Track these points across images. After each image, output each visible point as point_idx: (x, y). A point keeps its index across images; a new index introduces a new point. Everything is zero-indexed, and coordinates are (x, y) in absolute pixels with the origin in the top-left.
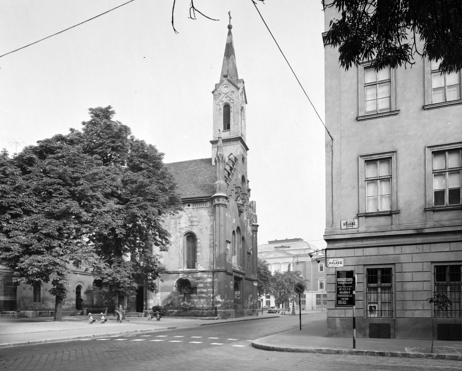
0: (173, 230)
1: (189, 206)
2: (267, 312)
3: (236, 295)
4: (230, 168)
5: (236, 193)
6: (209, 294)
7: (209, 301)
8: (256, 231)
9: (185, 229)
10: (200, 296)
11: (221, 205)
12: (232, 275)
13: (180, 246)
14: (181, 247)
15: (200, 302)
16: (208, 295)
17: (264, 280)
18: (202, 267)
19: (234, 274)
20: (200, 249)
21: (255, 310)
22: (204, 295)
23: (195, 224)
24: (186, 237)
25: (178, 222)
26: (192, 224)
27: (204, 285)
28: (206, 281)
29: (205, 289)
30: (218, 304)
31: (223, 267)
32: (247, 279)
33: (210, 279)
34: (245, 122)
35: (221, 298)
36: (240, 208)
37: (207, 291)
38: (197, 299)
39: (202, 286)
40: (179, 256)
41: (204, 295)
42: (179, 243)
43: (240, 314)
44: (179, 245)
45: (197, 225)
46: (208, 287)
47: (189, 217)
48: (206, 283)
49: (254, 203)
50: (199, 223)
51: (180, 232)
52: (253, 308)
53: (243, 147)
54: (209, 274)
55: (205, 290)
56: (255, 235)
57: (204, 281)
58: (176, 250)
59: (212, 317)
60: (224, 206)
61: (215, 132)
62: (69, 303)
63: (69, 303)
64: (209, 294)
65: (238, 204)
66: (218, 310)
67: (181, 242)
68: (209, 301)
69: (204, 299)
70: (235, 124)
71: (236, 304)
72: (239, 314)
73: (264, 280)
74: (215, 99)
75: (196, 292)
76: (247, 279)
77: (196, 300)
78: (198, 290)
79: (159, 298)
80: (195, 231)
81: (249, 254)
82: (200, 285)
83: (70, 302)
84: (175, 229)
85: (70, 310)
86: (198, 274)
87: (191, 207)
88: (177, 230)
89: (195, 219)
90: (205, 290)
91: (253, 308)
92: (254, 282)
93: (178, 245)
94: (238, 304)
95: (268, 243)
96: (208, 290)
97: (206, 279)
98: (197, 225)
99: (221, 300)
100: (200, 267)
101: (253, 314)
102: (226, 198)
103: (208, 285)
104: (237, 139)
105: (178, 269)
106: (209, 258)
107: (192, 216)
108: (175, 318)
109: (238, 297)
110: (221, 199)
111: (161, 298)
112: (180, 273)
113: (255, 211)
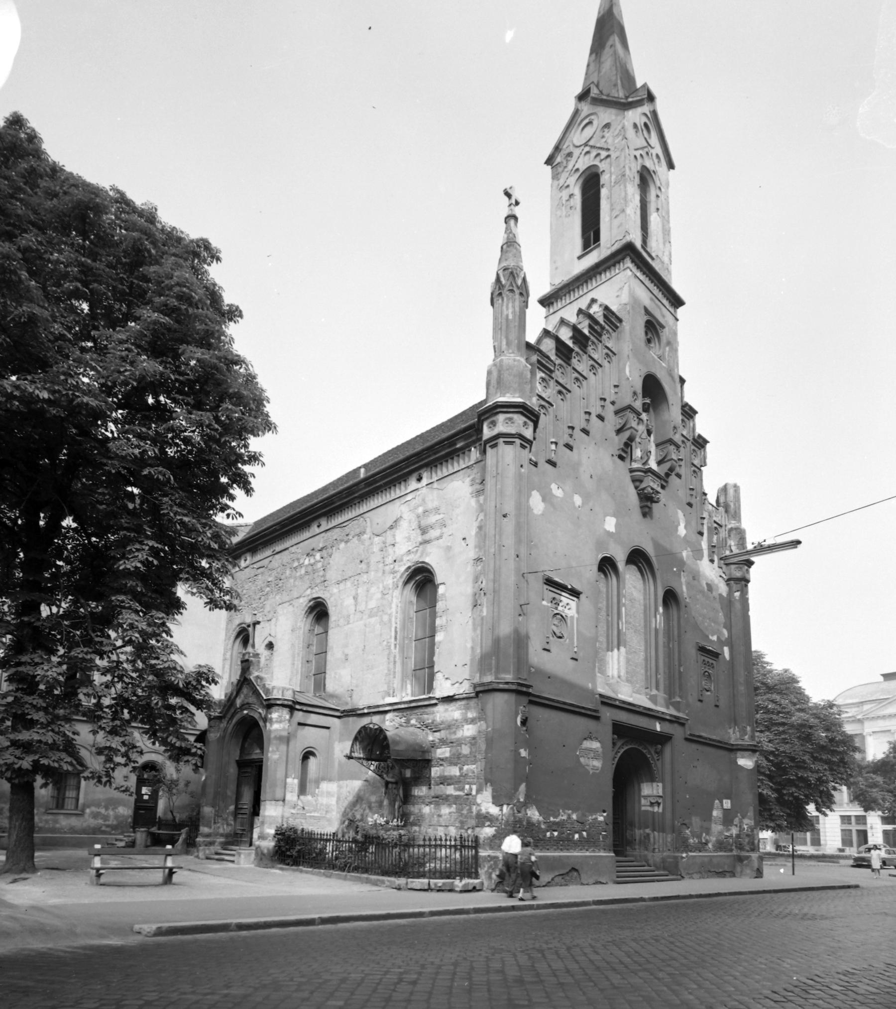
0: (377, 571)
1: (419, 479)
2: (851, 862)
3: (646, 797)
4: (570, 334)
5: (619, 431)
6: (467, 787)
7: (465, 812)
8: (745, 581)
9: (405, 558)
10: (439, 793)
11: (501, 440)
12: (597, 718)
13: (390, 620)
14: (396, 621)
15: (440, 816)
16: (462, 789)
17: (827, 762)
18: (449, 683)
19: (608, 715)
20: (444, 618)
21: (748, 858)
22: (450, 790)
23: (433, 534)
24: (410, 585)
25: (390, 540)
26: (427, 537)
27: (454, 750)
28: (460, 734)
29: (456, 765)
30: (483, 826)
31: (508, 672)
32: (692, 740)
33: (470, 726)
34: (666, 220)
35: (497, 801)
36: (643, 486)
37: (461, 776)
38: (431, 803)
39: (448, 755)
40: (386, 652)
41: (450, 790)
42: (391, 608)
43: (664, 869)
44: (390, 615)
45: (440, 537)
46: (465, 756)
47: (418, 517)
48: (459, 743)
49: (731, 492)
50: (444, 530)
51: (394, 572)
52: (741, 847)
53: (656, 291)
54: (467, 708)
55: (454, 771)
56: (737, 594)
57: (453, 737)
58: (381, 635)
59: (440, 882)
60: (518, 441)
61: (556, 268)
62: (103, 811)
63: (103, 811)
64: (467, 787)
65: (631, 471)
66: (483, 853)
67: (394, 606)
68: (465, 812)
69: (450, 806)
70: (615, 213)
71: (648, 831)
72: (658, 869)
73: (827, 762)
74: (555, 177)
75: (429, 778)
76: (692, 740)
77: (426, 810)
78: (435, 772)
79: (333, 801)
80: (433, 558)
81: (709, 654)
82: (443, 752)
83: (107, 808)
84: (381, 565)
85: (104, 832)
86: (436, 709)
87: (425, 481)
88: (387, 568)
89: (433, 519)
90: (454, 771)
91: (741, 847)
92: (739, 754)
93: (386, 618)
94: (654, 830)
95: (882, 679)
96: (465, 768)
97: (458, 727)
98: (440, 537)
99: (494, 810)
100: (443, 688)
101: (738, 869)
102: (532, 416)
103: (465, 750)
104: (619, 257)
105: (383, 698)
106: (469, 645)
107: (425, 512)
108: (339, 877)
109: (652, 804)
110: (501, 417)
111: (338, 799)
112: (386, 712)
113: (737, 516)
